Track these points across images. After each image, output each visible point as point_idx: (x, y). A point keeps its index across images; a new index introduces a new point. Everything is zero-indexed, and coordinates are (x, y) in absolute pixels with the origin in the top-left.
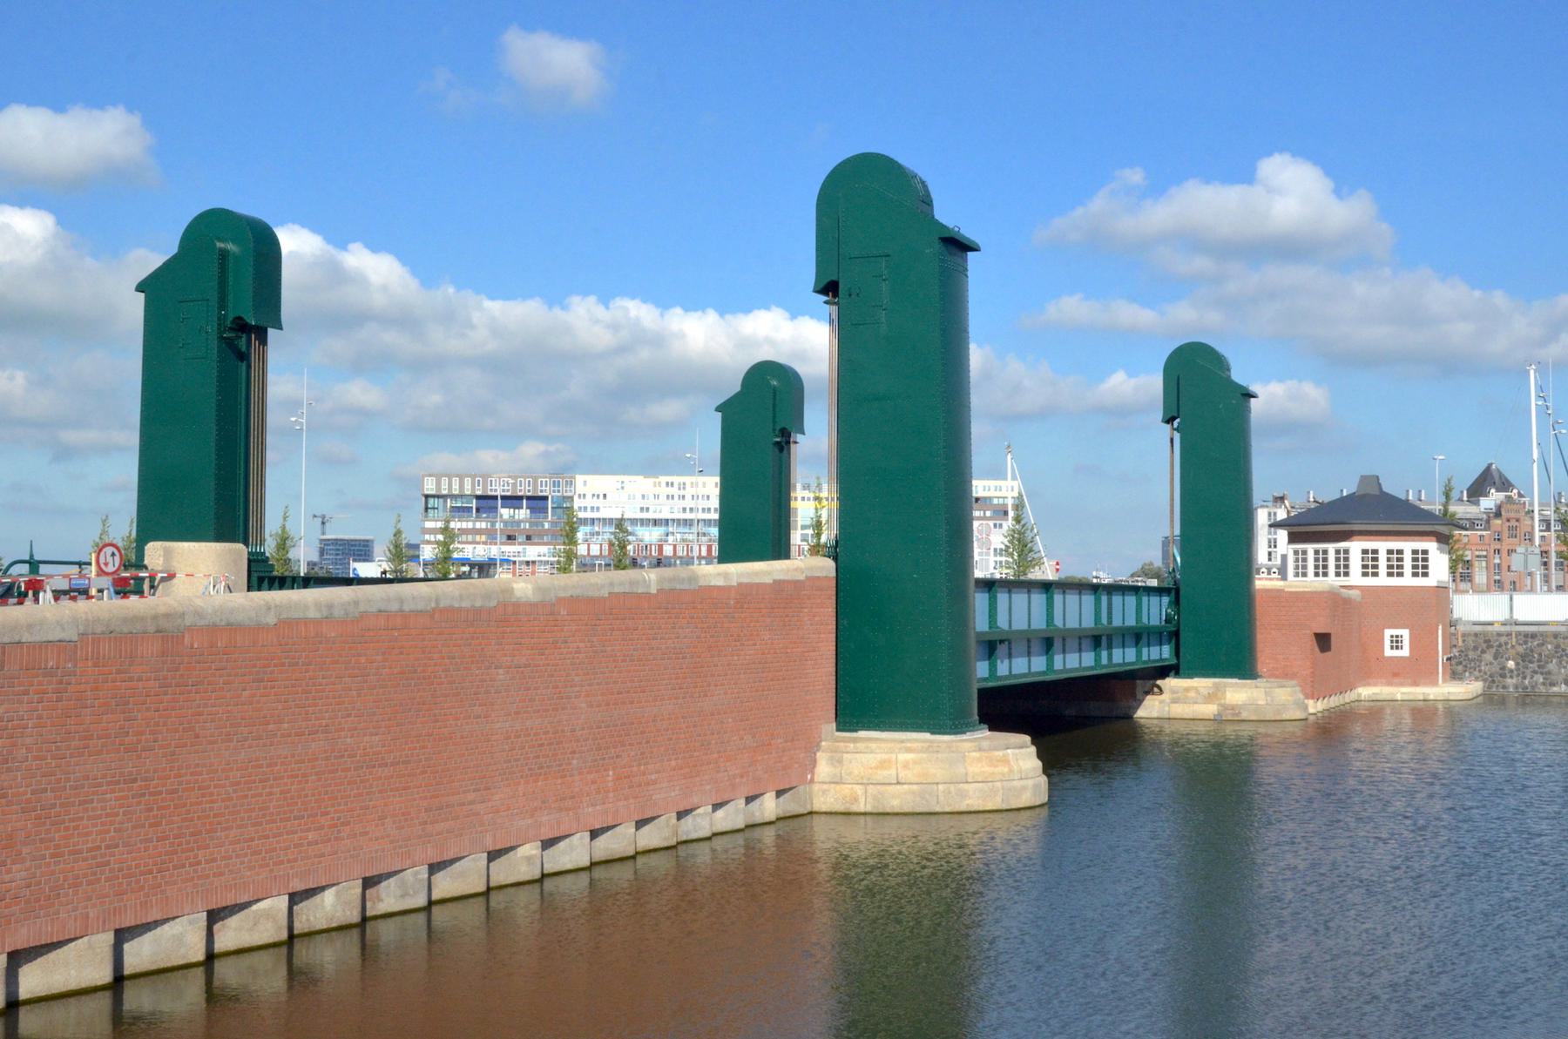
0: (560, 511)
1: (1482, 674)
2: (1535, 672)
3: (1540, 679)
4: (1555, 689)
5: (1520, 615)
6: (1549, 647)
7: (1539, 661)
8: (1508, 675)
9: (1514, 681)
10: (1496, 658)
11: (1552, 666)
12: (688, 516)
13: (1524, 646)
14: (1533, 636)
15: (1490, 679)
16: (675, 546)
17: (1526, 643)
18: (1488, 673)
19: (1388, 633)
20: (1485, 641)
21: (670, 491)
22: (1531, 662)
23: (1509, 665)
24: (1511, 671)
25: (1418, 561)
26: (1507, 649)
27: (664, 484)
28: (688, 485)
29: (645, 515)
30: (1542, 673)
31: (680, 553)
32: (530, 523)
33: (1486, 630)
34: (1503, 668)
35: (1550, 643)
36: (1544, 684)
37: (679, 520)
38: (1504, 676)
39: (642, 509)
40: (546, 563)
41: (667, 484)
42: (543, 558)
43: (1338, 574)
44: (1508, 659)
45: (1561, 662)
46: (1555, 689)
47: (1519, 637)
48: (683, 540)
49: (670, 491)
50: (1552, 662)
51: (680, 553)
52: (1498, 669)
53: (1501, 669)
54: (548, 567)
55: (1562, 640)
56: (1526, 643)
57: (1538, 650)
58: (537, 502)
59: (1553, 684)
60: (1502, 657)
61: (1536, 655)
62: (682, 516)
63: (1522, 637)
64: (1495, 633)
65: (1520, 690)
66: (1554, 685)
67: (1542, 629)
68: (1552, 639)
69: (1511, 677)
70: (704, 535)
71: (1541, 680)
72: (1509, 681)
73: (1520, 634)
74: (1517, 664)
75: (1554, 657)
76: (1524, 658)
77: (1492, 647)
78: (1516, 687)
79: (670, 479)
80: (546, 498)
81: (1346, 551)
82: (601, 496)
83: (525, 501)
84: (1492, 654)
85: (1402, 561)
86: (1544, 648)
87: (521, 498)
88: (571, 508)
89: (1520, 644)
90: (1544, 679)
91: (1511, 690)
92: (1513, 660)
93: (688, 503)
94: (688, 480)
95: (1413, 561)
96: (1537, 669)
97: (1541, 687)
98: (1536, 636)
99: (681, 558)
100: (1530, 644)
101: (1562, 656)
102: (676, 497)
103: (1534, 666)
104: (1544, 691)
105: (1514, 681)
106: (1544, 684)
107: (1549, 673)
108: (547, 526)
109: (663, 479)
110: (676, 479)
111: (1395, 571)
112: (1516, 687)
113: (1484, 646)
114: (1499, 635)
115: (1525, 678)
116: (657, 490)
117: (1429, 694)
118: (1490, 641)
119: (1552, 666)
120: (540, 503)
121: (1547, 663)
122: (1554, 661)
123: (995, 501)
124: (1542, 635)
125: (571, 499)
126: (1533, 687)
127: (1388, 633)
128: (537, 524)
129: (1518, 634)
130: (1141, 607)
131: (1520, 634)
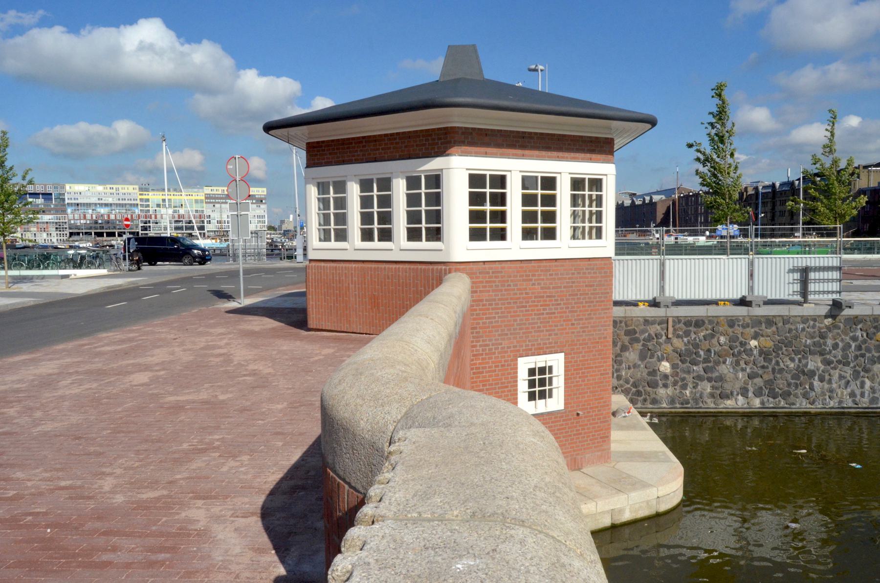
0: (58, 200)
1: (621, 382)
2: (699, 378)
3: (706, 387)
4: (729, 403)
5: (676, 290)
6: (722, 339)
7: (706, 360)
8: (660, 383)
9: (670, 391)
10: (642, 357)
11: (725, 369)
12: (121, 202)
13: (685, 339)
14: (699, 323)
15: (634, 390)
16: (115, 215)
17: (687, 334)
18: (632, 380)
19: (524, 364)
20: (627, 333)
21: (112, 191)
22: (694, 363)
23: (662, 369)
24: (666, 377)
25: (543, 212)
26: (660, 344)
27: (109, 188)
28: (120, 189)
29: (100, 202)
30: (710, 380)
31: (118, 218)
32: (44, 205)
33: (629, 314)
34: (653, 372)
35: (722, 334)
36: (712, 395)
37: (117, 204)
38: (653, 385)
39: (99, 199)
40: (53, 223)
41: (110, 188)
42: (51, 221)
43: (367, 236)
44: (660, 360)
45: (737, 363)
46: (729, 403)
47: (678, 326)
48: (119, 213)
49: (112, 191)
50: (724, 362)
51: (118, 218)
52: (645, 374)
53: (649, 374)
54: (55, 224)
55: (740, 329)
56: (687, 334)
57: (706, 345)
58: (47, 196)
59: (724, 396)
60: (652, 356)
61: (702, 353)
62: (118, 202)
63: (682, 325)
64: (642, 320)
65: (678, 405)
66: (728, 397)
67: (712, 311)
68: (726, 327)
69: (665, 386)
70: (129, 210)
71: (709, 390)
72: (662, 391)
73: (680, 322)
74: (674, 366)
75: (727, 355)
76: (685, 357)
77: (637, 340)
78: (672, 401)
79: (111, 186)
80: (51, 194)
81: (435, 180)
82: (79, 194)
83: (41, 196)
84: (638, 352)
85: (525, 214)
86: (714, 341)
87: (39, 194)
88: (64, 200)
89: (678, 336)
90: (713, 387)
91: (664, 405)
92: (667, 360)
93: (121, 196)
94: (120, 186)
95: (472, 221)
96: (702, 373)
97: (709, 401)
98: (703, 322)
99: (118, 220)
100: (693, 336)
101: (740, 353)
102: (115, 194)
103: (698, 369)
104: (712, 405)
105: (670, 391)
106: (712, 395)
107: (721, 379)
108: (52, 206)
109: (108, 186)
110: (115, 186)
111: (540, 225)
112: (672, 401)
113: (626, 339)
114: (647, 322)
115: (684, 387)
116: (106, 191)
117: (621, 511)
118: (635, 332)
119: (725, 369)
120: (49, 196)
121: (717, 363)
122: (729, 361)
123: (257, 196)
124: (710, 322)
125: (64, 194)
126: (696, 401)
127: (524, 364)
128: (47, 205)
129: (677, 320)
130: (38, 293)
131: (680, 322)
